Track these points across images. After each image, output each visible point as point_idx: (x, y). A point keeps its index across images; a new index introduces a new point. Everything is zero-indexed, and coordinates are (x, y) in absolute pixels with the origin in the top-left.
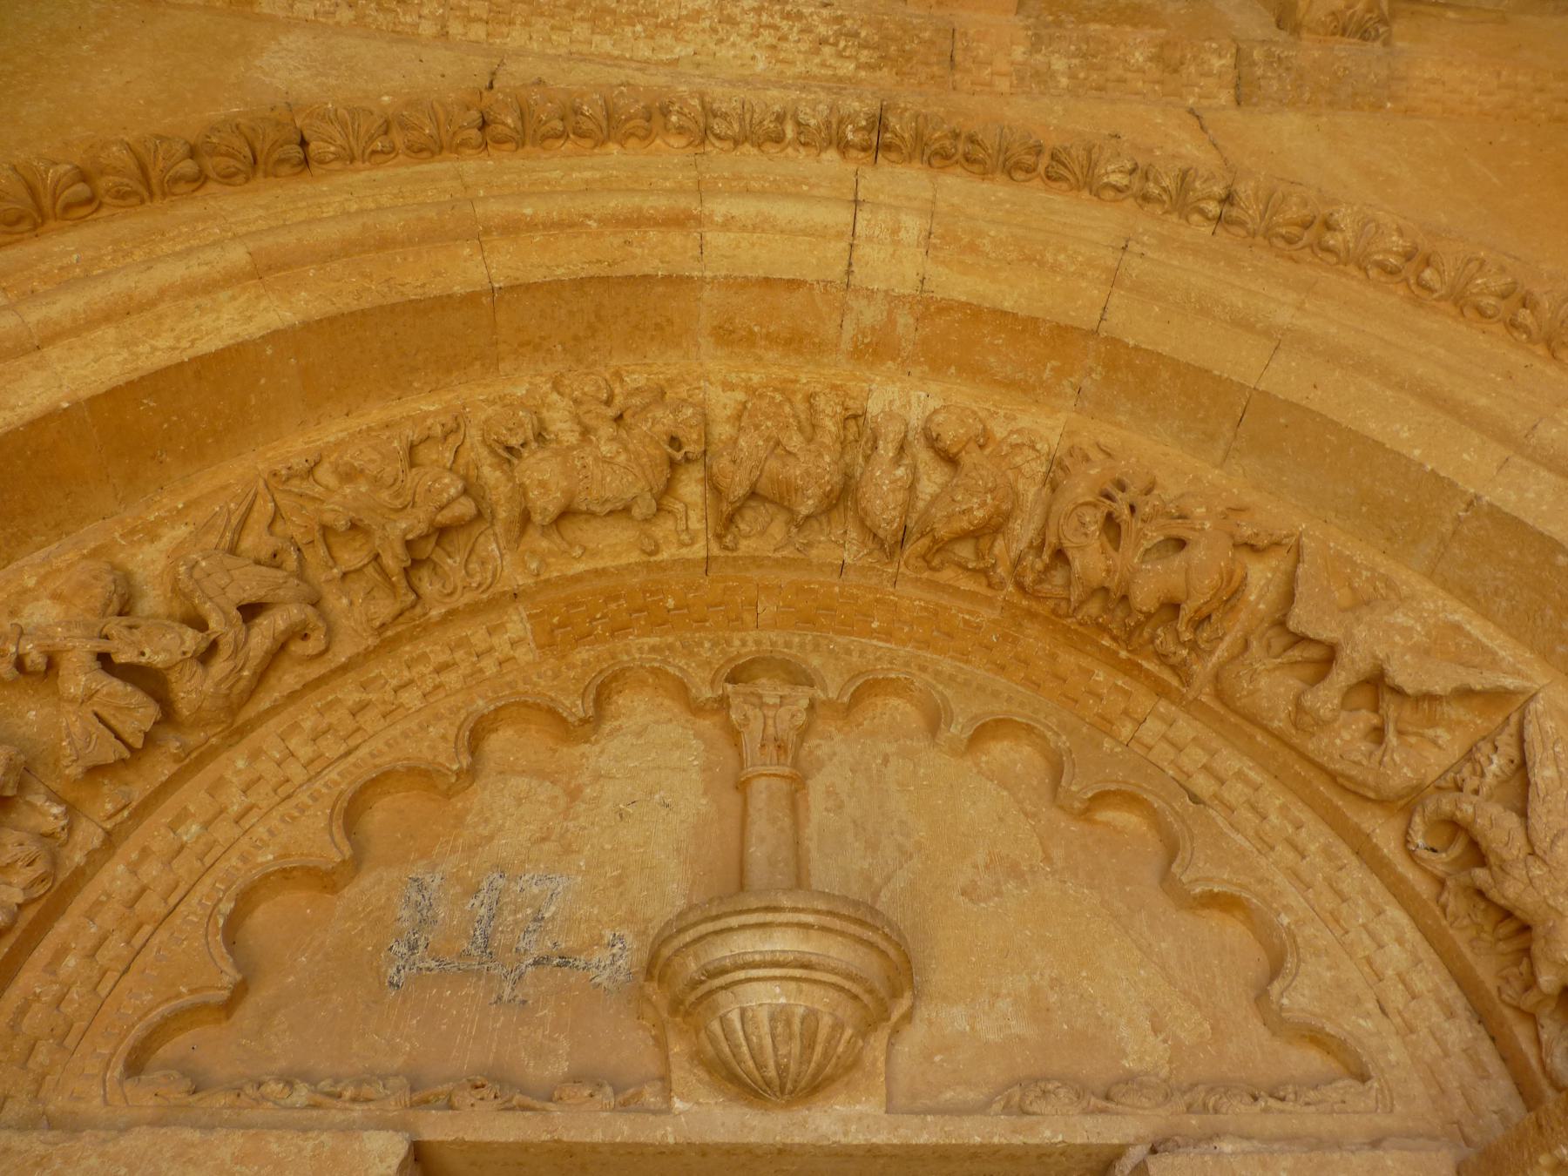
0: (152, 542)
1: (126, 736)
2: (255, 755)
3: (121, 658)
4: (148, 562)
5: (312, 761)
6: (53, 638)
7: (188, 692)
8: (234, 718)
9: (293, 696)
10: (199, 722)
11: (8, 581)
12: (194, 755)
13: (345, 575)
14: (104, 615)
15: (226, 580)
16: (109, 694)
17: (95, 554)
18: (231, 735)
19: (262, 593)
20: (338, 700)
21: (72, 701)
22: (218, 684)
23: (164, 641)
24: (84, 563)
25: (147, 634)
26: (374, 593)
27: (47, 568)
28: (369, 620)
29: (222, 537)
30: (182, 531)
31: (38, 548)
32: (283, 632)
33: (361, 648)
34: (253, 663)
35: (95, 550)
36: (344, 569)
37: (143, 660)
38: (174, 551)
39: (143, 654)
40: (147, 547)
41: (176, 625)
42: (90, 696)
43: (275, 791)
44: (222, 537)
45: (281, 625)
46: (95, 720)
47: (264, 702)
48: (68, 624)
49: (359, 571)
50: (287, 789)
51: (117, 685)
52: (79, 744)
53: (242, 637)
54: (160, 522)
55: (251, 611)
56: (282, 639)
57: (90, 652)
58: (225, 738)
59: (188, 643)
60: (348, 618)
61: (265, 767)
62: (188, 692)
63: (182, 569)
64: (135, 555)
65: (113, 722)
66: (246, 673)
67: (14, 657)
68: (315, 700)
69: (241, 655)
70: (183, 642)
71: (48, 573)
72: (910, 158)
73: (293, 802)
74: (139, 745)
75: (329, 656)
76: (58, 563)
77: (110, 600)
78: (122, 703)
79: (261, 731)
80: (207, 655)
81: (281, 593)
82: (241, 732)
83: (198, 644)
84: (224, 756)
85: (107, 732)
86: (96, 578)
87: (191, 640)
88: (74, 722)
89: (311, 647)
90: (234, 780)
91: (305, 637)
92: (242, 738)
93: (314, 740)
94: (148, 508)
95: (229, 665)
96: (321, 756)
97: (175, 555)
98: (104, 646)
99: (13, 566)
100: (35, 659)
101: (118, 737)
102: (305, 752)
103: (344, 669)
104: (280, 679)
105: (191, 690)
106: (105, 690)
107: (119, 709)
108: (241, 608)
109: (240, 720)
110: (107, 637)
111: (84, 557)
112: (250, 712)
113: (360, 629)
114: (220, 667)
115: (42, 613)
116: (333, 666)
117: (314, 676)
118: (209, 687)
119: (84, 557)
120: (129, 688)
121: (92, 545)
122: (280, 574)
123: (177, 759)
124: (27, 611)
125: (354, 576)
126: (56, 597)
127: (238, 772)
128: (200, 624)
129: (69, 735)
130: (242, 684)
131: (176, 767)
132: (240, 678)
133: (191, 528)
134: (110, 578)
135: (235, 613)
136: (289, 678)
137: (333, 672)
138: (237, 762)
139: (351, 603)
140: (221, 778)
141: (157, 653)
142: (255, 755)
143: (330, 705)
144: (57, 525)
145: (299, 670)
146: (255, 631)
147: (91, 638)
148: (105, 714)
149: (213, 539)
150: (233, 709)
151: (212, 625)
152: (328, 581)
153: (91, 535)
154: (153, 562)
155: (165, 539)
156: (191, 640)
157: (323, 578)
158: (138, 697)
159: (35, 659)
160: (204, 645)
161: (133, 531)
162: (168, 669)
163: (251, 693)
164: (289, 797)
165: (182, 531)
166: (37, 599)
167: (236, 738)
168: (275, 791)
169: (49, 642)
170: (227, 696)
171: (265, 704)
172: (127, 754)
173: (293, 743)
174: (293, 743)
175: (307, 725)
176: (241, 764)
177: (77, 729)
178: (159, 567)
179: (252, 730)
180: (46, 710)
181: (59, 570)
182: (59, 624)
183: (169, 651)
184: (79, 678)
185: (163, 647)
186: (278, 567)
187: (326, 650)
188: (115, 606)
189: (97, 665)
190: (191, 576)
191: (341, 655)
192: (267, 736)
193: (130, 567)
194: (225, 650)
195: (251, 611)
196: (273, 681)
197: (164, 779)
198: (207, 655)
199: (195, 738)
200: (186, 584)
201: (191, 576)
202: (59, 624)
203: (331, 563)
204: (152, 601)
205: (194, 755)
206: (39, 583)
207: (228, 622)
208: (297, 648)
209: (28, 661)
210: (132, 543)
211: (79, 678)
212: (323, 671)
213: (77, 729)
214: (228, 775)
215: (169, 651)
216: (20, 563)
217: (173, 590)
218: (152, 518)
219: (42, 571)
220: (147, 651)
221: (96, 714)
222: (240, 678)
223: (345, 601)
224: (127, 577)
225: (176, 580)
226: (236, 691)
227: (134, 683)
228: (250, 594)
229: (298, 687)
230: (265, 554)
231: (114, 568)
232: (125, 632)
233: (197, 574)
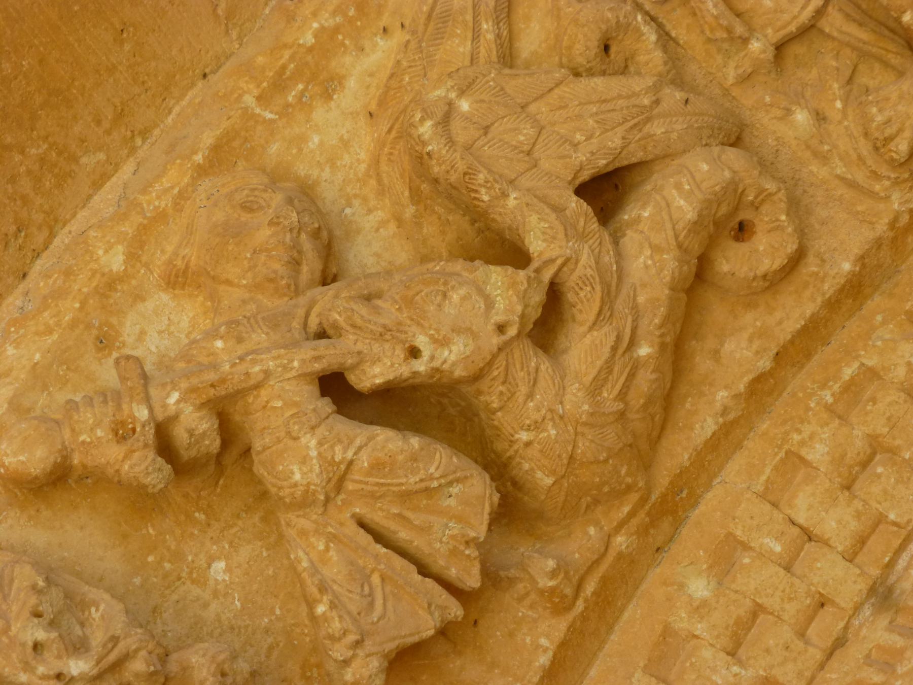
0: (327, 96)
1: (439, 563)
2: (725, 557)
3: (372, 376)
4: (334, 142)
5: (862, 541)
6: (214, 367)
7: (537, 426)
8: (650, 481)
9: (761, 391)
10: (581, 502)
11: (68, 273)
12: (590, 587)
13: (780, 48)
14: (297, 292)
15: (527, 132)
16: (377, 467)
17: (220, 158)
18: (654, 520)
19: (615, 141)
20: (872, 374)
21: (304, 503)
22: (595, 389)
23: (450, 309)
24: (206, 184)
25: (409, 302)
26: (863, 79)
27: (137, 219)
28: (880, 146)
29: (476, 35)
30: (381, 52)
31: (97, 185)
32: (696, 226)
33: (882, 227)
34: (651, 322)
35: (216, 148)
36: (773, 35)
37: (421, 366)
38: (382, 103)
39: (414, 353)
40: (319, 114)
41: (459, 266)
42: (338, 481)
43: (801, 634)
44: (476, 35)
45: (685, 209)
46: (365, 538)
47: (701, 422)
48: (235, 330)
49: (808, 30)
50: (825, 627)
51: (387, 441)
52: (354, 604)
53: (608, 258)
54: (328, 42)
55: (605, 192)
56: (696, 248)
57: (302, 376)
58: (643, 531)
59: (500, 304)
60: (824, 159)
61: (758, 580)
62: (537, 426)
63: (426, 129)
64: (302, 139)
65: (403, 535)
66: (644, 351)
67: (150, 431)
68: (813, 386)
69: (621, 305)
70: (490, 304)
71: (143, 230)
72: (803, 109)
73: (855, 652)
74: (473, 580)
75: (811, 266)
76: (155, 200)
77: (296, 246)
78: (412, 481)
79: (711, 502)
80: (547, 323)
81: (657, 129)
82: (668, 511)
83: (524, 297)
84: (655, 575)
85: (399, 562)
86: (248, 207)
87: (505, 294)
88: (321, 551)
89: (765, 251)
90: (699, 628)
91: (742, 231)
92: (677, 525)
93: (848, 487)
94: (290, 18)
95: (604, 337)
96: (881, 519)
97: (391, 106)
98: (329, 355)
99: (62, 239)
100: (195, 426)
101: (424, 571)
102: (838, 523)
103: (855, 290)
104: (716, 354)
105: (549, 412)
106: (364, 461)
107: (405, 496)
108: (582, 191)
109: (663, 480)
110: (322, 335)
111: (202, 171)
112: (677, 452)
113: (860, 176)
114: (585, 345)
115: (160, 326)
116: (829, 288)
117: (793, 325)
118: (575, 400)
119: (202, 171)
120: (415, 442)
121: (208, 139)
122: (638, 84)
123: (559, 604)
124: (129, 329)
125: (797, 49)
126: (178, 279)
127: (700, 609)
128: (514, 255)
129: (323, 588)
130: (645, 381)
131: (560, 627)
132: (635, 368)
133: (399, 37)
134: (278, 199)
135: (575, 204)
136: (737, 350)
137: (833, 304)
138: (687, 585)
139: (820, 117)
140: (667, 632)
141: (442, 342)
142: (725, 557)
143: (852, 391)
144: (119, 116)
145: (750, 319)
146: (631, 240)
147: (295, 344)
148: (378, 517)
149: (457, 47)
150: (643, 450)
151: (535, 245)
152: (745, 79)
153: (195, 120)
154: (345, 144)
155: (352, 83)
156: (505, 294)
157: (731, 74)
158: (441, 460)
159: (195, 426)
160: (538, 297)
161: (280, 84)
162: (477, 377)
163: (667, 402)
164: (840, 643)
165: (381, 52)
166: (138, 297)
167: (666, 525)
168: (801, 634)
169: (211, 376)
170: (622, 415)
171: (706, 426)
172: (456, 610)
173: (804, 505)
174: (804, 505)
175: (817, 453)
176: (700, 587)
177: (335, 569)
178: (361, 153)
179: (694, 501)
180: (245, 553)
181: (161, 217)
182: (212, 334)
183: (469, 331)
184: (301, 446)
185: (456, 323)
186: (624, 71)
187: (797, 259)
188: (311, 266)
189: (326, 405)
190: (451, 142)
191: (839, 256)
192: (732, 499)
193: (301, 169)
194: (583, 303)
195: (605, 192)
196: (702, 364)
197: (544, 660)
198: (547, 323)
199: (583, 540)
200: (447, 161)
201: (451, 142)
202: (212, 334)
203: (740, 29)
204: (376, 240)
205: (590, 587)
206: (132, 257)
207: (570, 230)
208: (735, 262)
209: (180, 435)
210: (285, 112)
211: (301, 446)
212: (810, 309)
213: (335, 569)
214: (682, 621)
215: (469, 331)
216: (74, 226)
217: (416, 196)
218: (309, 39)
219: (128, 228)
220: (421, 341)
221: (362, 525)
222: (635, 368)
223: (801, 117)
224: (305, 194)
225: (421, 161)
226: (636, 400)
227: (416, 426)
228: (593, 154)
229: (765, 364)
230: (584, 47)
231: (275, 177)
232: (362, 310)
233: (461, 133)
